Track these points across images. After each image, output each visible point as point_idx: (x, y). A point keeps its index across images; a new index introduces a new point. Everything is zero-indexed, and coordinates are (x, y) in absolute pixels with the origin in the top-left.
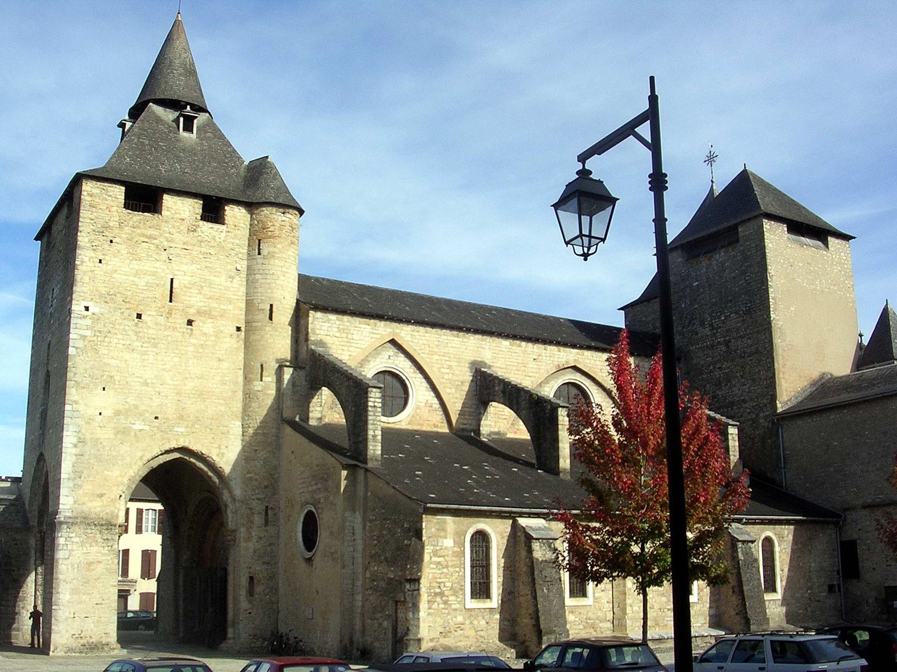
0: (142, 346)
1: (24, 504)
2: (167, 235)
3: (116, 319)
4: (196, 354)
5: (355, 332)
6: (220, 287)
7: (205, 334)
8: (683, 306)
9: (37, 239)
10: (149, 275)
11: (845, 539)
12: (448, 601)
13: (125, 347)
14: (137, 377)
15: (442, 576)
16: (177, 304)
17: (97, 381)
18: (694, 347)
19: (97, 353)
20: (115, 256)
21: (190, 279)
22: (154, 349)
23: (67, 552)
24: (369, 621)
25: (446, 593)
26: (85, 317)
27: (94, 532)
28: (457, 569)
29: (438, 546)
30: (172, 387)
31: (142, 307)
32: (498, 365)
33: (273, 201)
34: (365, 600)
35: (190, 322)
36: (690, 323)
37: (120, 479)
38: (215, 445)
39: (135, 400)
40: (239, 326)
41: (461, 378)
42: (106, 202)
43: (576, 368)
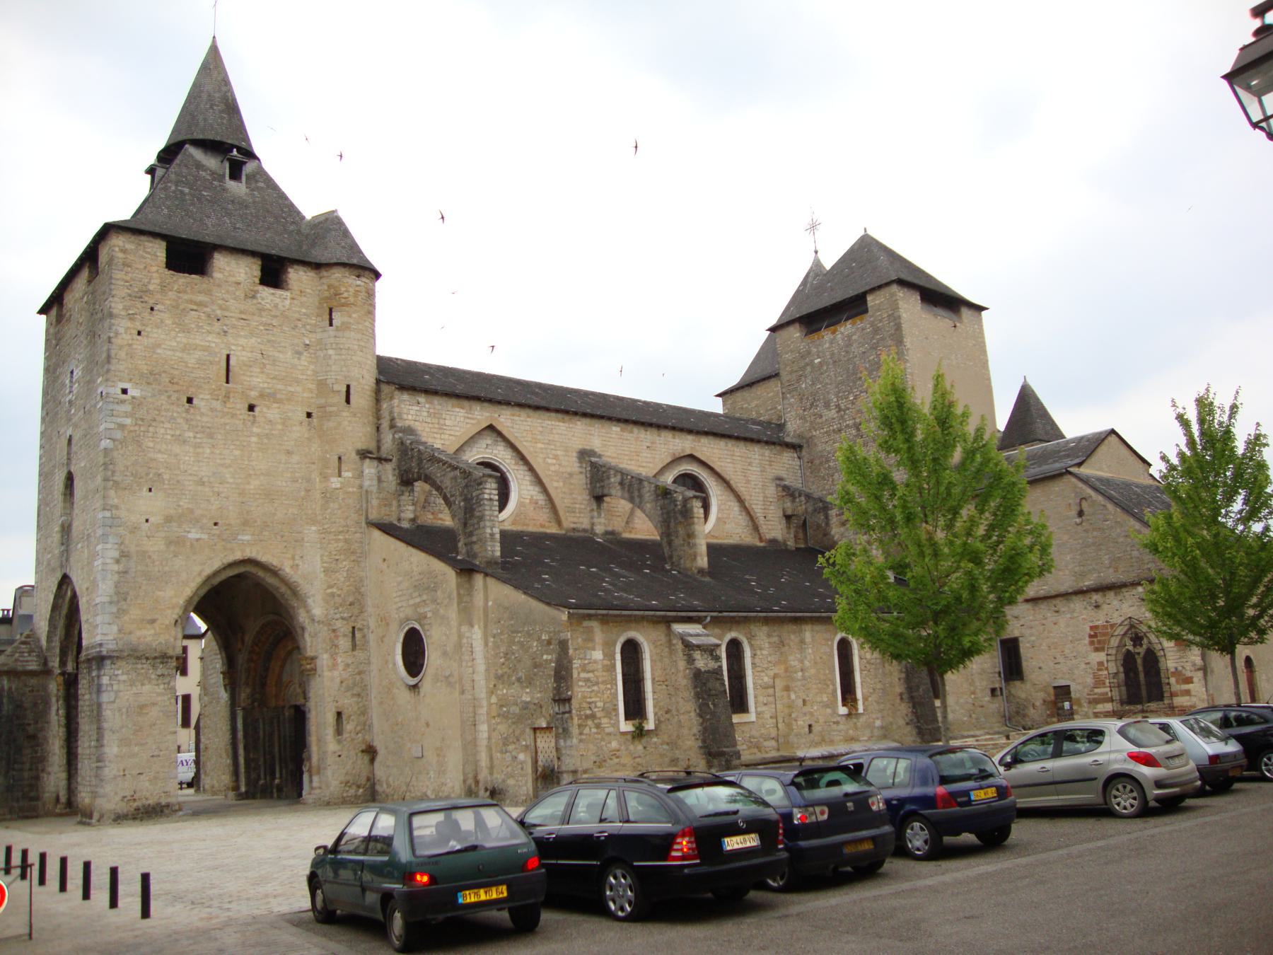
0: (195, 437)
1: (38, 640)
2: (220, 302)
3: (162, 405)
4: (260, 446)
5: (448, 417)
6: (285, 365)
7: (270, 421)
8: (803, 386)
9: (42, 311)
10: (200, 350)
11: (1004, 637)
12: (600, 724)
13: (174, 438)
14: (191, 475)
15: (593, 694)
16: (235, 386)
17: (141, 480)
18: (818, 432)
19: (140, 446)
20: (158, 327)
21: (249, 355)
22: (210, 441)
23: (112, 694)
24: (498, 754)
25: (598, 715)
26: (123, 402)
27: (144, 667)
28: (609, 686)
29: (586, 659)
30: (234, 486)
31: (194, 390)
32: (609, 454)
33: (347, 262)
34: (492, 730)
35: (251, 408)
36: (812, 405)
37: (174, 601)
38: (289, 556)
39: (189, 503)
40: (310, 411)
41: (569, 470)
42: (144, 261)
43: (692, 458)
